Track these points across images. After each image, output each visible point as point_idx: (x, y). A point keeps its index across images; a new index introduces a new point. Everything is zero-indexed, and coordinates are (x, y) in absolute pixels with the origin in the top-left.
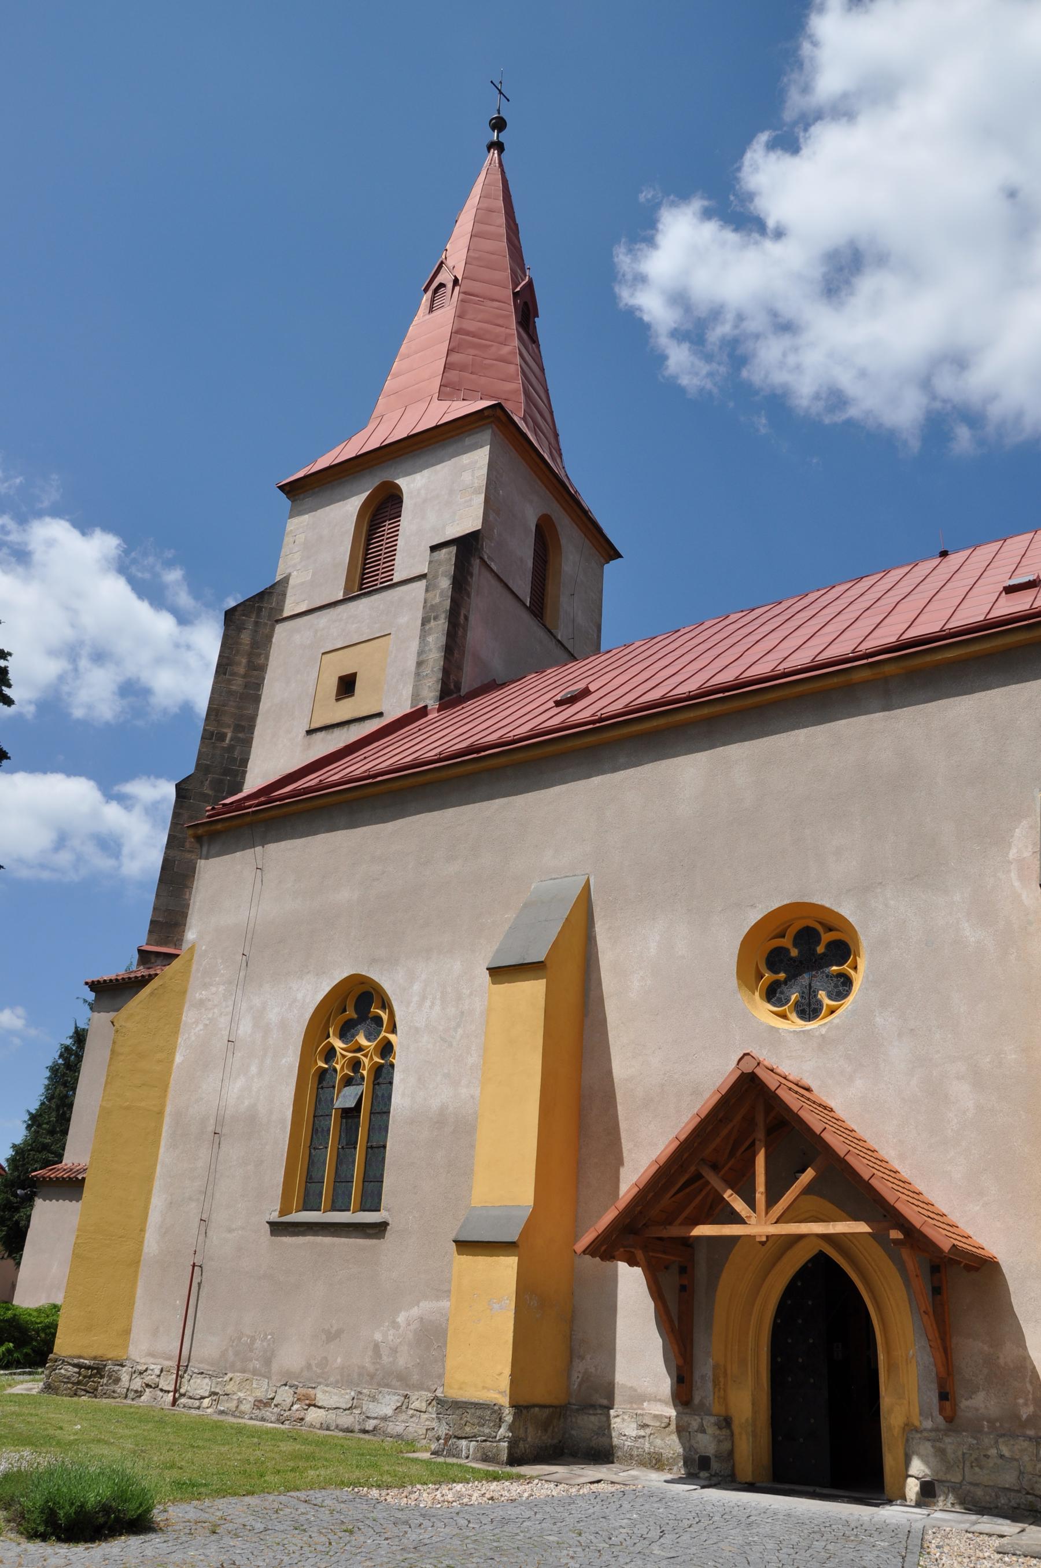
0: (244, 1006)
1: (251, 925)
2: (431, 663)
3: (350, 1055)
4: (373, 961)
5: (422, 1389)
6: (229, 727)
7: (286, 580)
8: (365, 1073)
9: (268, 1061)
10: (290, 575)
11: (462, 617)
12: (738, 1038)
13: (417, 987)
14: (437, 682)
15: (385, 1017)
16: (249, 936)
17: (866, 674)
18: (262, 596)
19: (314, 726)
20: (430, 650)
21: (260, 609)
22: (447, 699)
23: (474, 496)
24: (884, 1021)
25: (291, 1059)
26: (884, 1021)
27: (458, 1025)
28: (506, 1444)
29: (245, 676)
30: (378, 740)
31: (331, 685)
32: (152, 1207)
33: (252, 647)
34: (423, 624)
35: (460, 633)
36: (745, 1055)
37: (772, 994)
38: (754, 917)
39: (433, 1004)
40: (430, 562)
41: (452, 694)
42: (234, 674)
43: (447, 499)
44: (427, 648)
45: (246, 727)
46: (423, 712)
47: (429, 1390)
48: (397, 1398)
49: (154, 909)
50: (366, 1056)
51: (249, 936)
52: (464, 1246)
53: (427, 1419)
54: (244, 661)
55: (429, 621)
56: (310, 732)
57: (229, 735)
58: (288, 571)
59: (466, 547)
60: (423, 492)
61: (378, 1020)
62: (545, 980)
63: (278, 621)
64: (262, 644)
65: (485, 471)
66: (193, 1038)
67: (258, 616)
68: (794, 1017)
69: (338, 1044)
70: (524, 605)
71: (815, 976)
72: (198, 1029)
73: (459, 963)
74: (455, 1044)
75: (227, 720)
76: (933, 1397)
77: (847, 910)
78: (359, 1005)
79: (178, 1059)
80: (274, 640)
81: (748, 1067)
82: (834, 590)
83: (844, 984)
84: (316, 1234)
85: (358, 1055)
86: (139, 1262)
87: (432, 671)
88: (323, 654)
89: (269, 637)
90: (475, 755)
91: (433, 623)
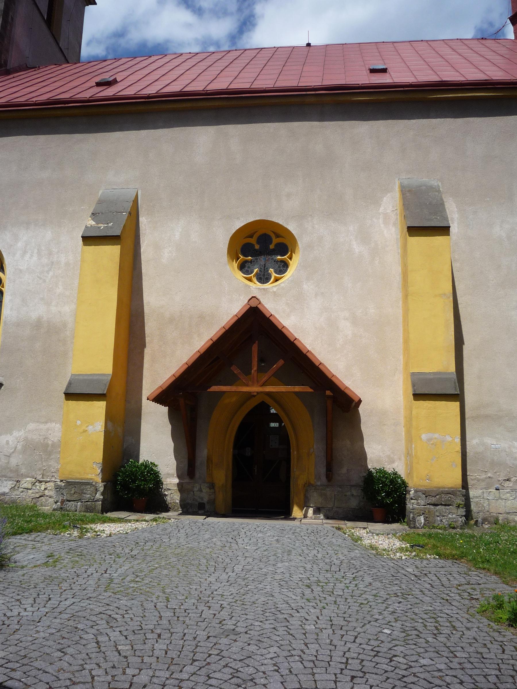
5: (28, 477)
12: (226, 289)
13: (20, 244)
17: (313, 100)
24: (308, 287)
26: (308, 287)
27: (50, 270)
28: (101, 502)
35: (8, 28)
36: (253, 297)
37: (242, 267)
38: (239, 224)
39: (32, 256)
47: (33, 477)
48: (11, 482)
52: (70, 396)
53: (33, 493)
68: (255, 280)
71: (268, 261)
73: (50, 232)
74: (47, 280)
76: (323, 470)
77: (292, 227)
81: (254, 304)
82: (136, 59)
83: (283, 266)
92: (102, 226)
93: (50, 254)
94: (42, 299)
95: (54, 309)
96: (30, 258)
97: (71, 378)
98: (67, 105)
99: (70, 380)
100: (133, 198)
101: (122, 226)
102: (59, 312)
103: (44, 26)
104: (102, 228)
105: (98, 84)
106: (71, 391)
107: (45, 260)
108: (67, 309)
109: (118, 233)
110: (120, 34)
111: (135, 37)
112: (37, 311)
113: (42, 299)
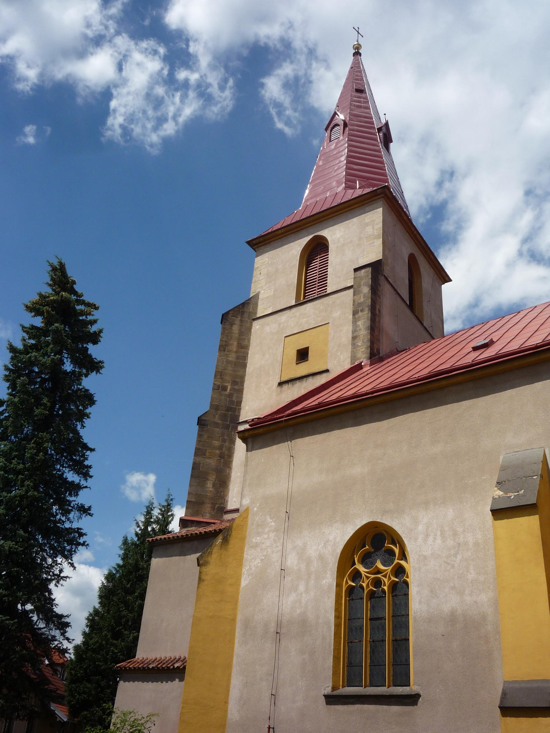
0: (289, 546)
1: (290, 493)
2: (362, 337)
3: (373, 576)
4: (385, 512)
6: (229, 382)
7: (257, 296)
8: (386, 588)
9: (312, 582)
10: (259, 293)
11: (377, 310)
13: (420, 528)
14: (367, 348)
15: (397, 551)
16: (289, 500)
18: (243, 305)
19: (284, 379)
20: (360, 330)
21: (243, 313)
22: (373, 358)
23: (375, 240)
25: (330, 579)
29: (236, 352)
30: (338, 382)
31: (293, 355)
32: (232, 686)
33: (240, 335)
34: (354, 315)
35: (377, 320)
39: (435, 538)
40: (355, 278)
41: (376, 356)
42: (229, 351)
43: (356, 242)
44: (358, 329)
45: (238, 384)
46: (359, 367)
49: (189, 493)
50: (385, 576)
51: (289, 500)
52: (507, 711)
54: (235, 343)
55: (358, 312)
56: (281, 384)
57: (229, 387)
58: (257, 291)
59: (376, 267)
60: (341, 240)
61: (391, 553)
62: (537, 517)
63: (254, 320)
64: (245, 333)
65: (381, 225)
66: (254, 569)
67: (242, 317)
69: (362, 569)
70: (407, 304)
72: (256, 563)
73: (451, 510)
74: (456, 565)
75: (227, 378)
78: (376, 543)
79: (244, 583)
80: (252, 331)
84: (363, 703)
85: (379, 576)
86: (225, 725)
87: (363, 342)
88: (285, 337)
89: (250, 329)
90: (447, 375)
91: (360, 314)
92: (512, 495)
93: (455, 534)
94: (453, 588)
95: (468, 599)
96: (434, 541)
97: (504, 686)
98: (450, 374)
99: (503, 689)
100: (541, 459)
101: (536, 492)
102: (475, 602)
103: (408, 311)
104: (513, 497)
105: (475, 349)
106: (508, 704)
107: (450, 543)
108: (484, 598)
109: (533, 500)
110: (475, 304)
111: (489, 304)
112: (450, 603)
113: (453, 588)
